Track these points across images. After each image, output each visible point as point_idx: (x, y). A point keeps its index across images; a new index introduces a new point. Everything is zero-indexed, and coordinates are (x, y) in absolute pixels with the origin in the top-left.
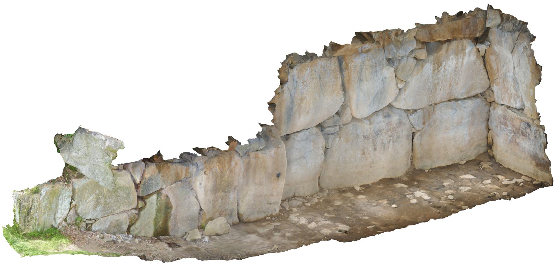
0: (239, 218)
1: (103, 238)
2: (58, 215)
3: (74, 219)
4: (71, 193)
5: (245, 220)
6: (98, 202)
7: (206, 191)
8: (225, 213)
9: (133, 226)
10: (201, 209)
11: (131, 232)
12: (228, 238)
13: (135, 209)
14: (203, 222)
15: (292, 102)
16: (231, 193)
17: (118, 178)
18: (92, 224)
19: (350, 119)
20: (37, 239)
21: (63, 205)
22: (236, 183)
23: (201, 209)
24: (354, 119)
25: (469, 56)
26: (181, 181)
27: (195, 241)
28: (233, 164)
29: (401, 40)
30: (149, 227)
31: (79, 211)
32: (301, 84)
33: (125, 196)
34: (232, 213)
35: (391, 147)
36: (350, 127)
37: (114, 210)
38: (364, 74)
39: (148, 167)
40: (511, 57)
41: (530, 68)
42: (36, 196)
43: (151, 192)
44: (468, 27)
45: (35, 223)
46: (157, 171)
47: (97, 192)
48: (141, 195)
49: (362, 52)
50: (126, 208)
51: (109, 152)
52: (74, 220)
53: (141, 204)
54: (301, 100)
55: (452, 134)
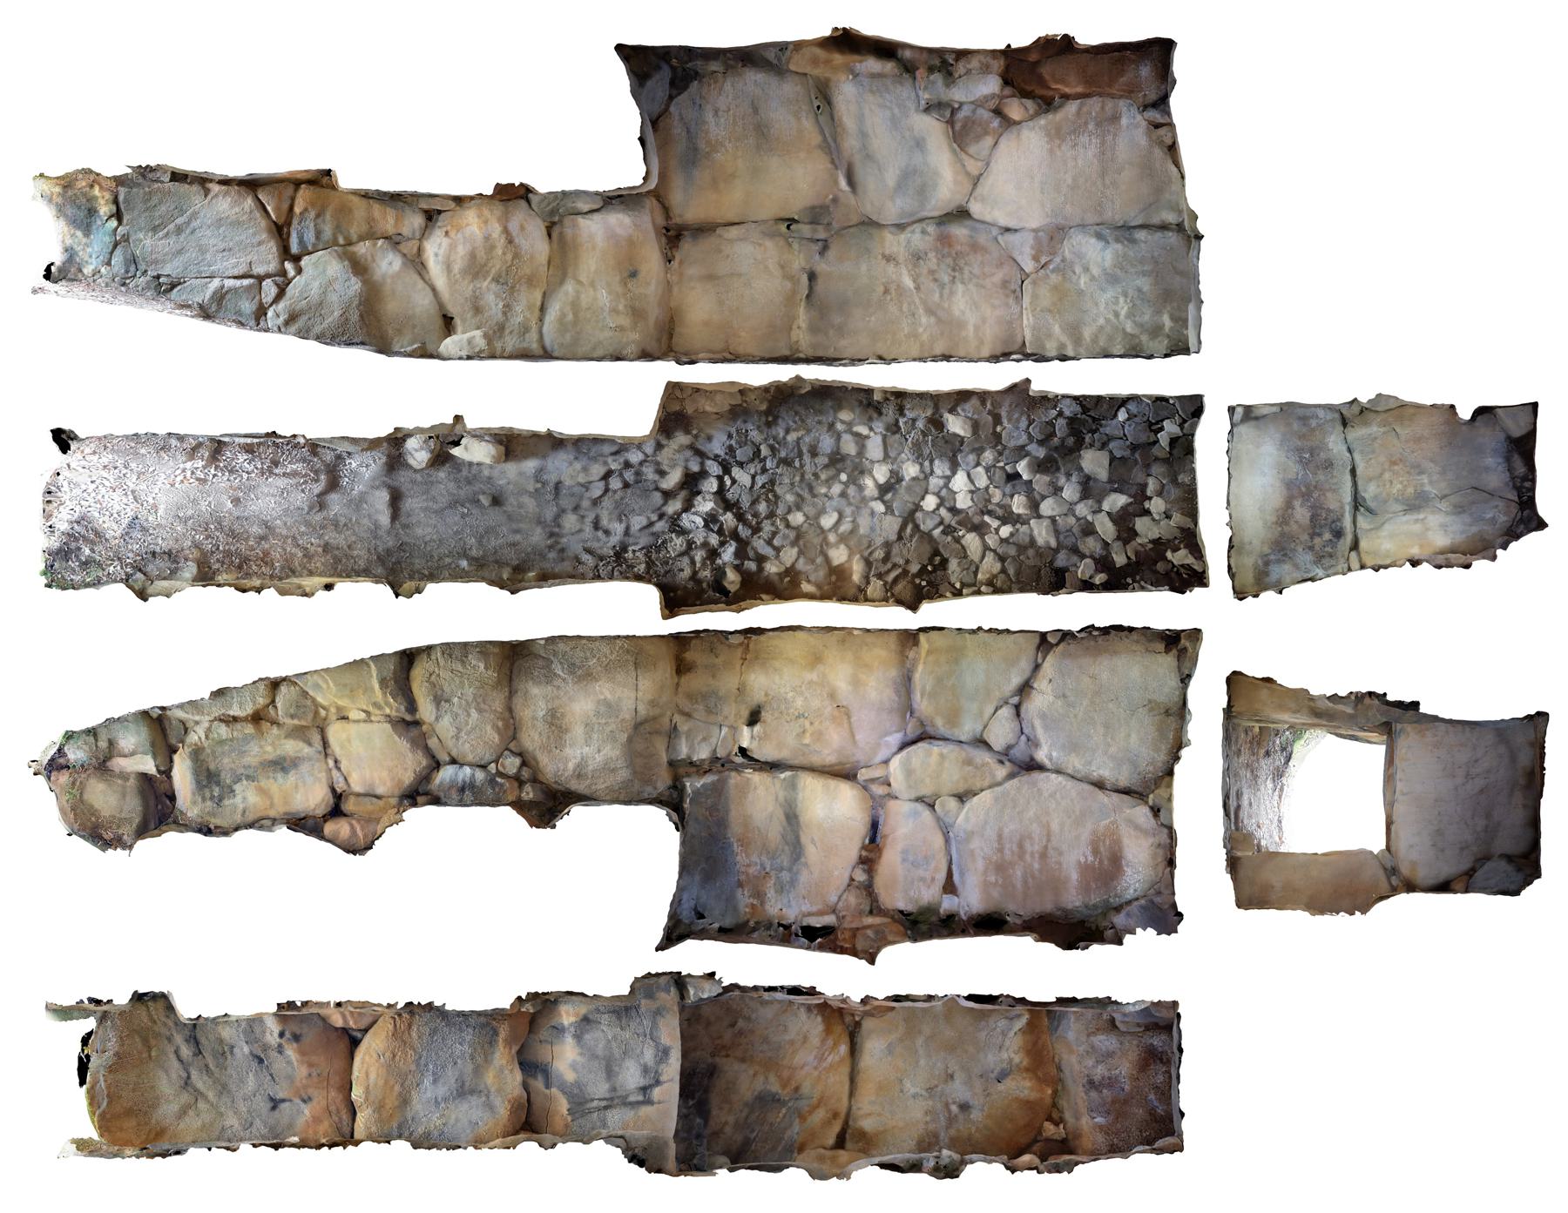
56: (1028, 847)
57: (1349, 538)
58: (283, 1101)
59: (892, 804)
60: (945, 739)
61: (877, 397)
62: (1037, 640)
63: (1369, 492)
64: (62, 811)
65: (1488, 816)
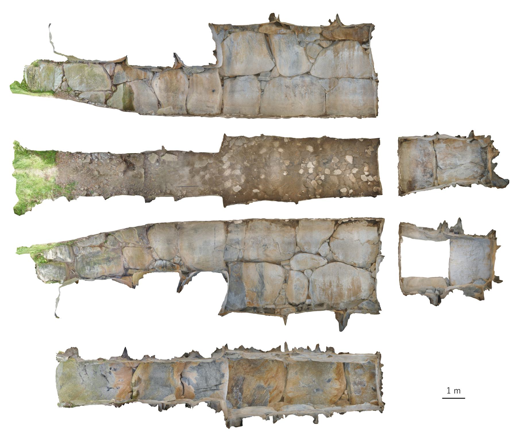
0: (187, 112)
2: (55, 84)
7: (160, 89)
15: (231, 54)
18: (79, 94)
19: (278, 75)
25: (358, 51)
28: (179, 77)
33: (101, 80)
36: (277, 79)
38: (282, 47)
42: (37, 68)
43: (120, 82)
44: (356, 33)
46: (122, 70)
49: (280, 33)
50: (104, 89)
54: (237, 54)
55: (351, 98)
56: (333, 284)
57: (435, 176)
58: (111, 388)
59: (291, 271)
60: (306, 252)
61: (286, 141)
62: (334, 223)
63: (440, 164)
64: (57, 386)
65: (477, 267)
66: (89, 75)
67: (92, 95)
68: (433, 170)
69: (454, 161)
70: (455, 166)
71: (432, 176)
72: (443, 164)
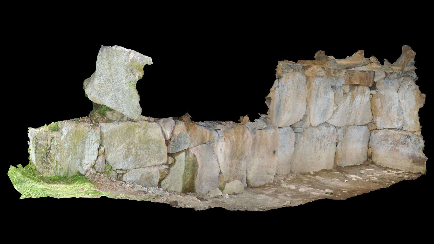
0: (247, 183)
1: (133, 187)
2: (85, 161)
3: (103, 166)
4: (99, 138)
5: (252, 185)
6: (129, 152)
8: (237, 178)
9: (164, 181)
10: (220, 173)
11: (162, 187)
12: (244, 197)
13: (166, 164)
14: (221, 184)
15: (280, 101)
16: (243, 162)
17: (149, 129)
18: (123, 174)
19: (309, 125)
20: (57, 183)
21: (90, 150)
22: (246, 154)
23: (220, 173)
24: (311, 125)
26: (205, 143)
27: (217, 197)
28: (245, 136)
29: (337, 76)
30: (178, 183)
31: (108, 159)
32: (286, 89)
33: (156, 149)
34: (242, 178)
35: (328, 149)
36: (309, 130)
37: (145, 163)
38: (319, 93)
39: (178, 124)
40: (397, 94)
41: (414, 98)
43: (180, 150)
45: (56, 167)
46: (185, 129)
47: (128, 141)
48: (171, 152)
49: (319, 76)
51: (135, 70)
52: (104, 168)
53: (171, 160)
54: (286, 101)
66: (140, 141)
67: (142, 175)
68: (402, 134)
69: (394, 110)
70: (400, 109)
71: (409, 137)
72: (397, 122)
